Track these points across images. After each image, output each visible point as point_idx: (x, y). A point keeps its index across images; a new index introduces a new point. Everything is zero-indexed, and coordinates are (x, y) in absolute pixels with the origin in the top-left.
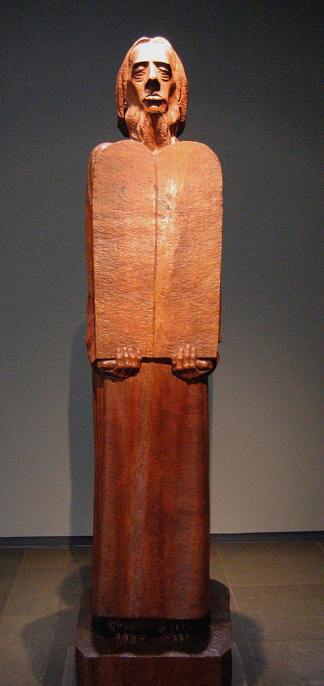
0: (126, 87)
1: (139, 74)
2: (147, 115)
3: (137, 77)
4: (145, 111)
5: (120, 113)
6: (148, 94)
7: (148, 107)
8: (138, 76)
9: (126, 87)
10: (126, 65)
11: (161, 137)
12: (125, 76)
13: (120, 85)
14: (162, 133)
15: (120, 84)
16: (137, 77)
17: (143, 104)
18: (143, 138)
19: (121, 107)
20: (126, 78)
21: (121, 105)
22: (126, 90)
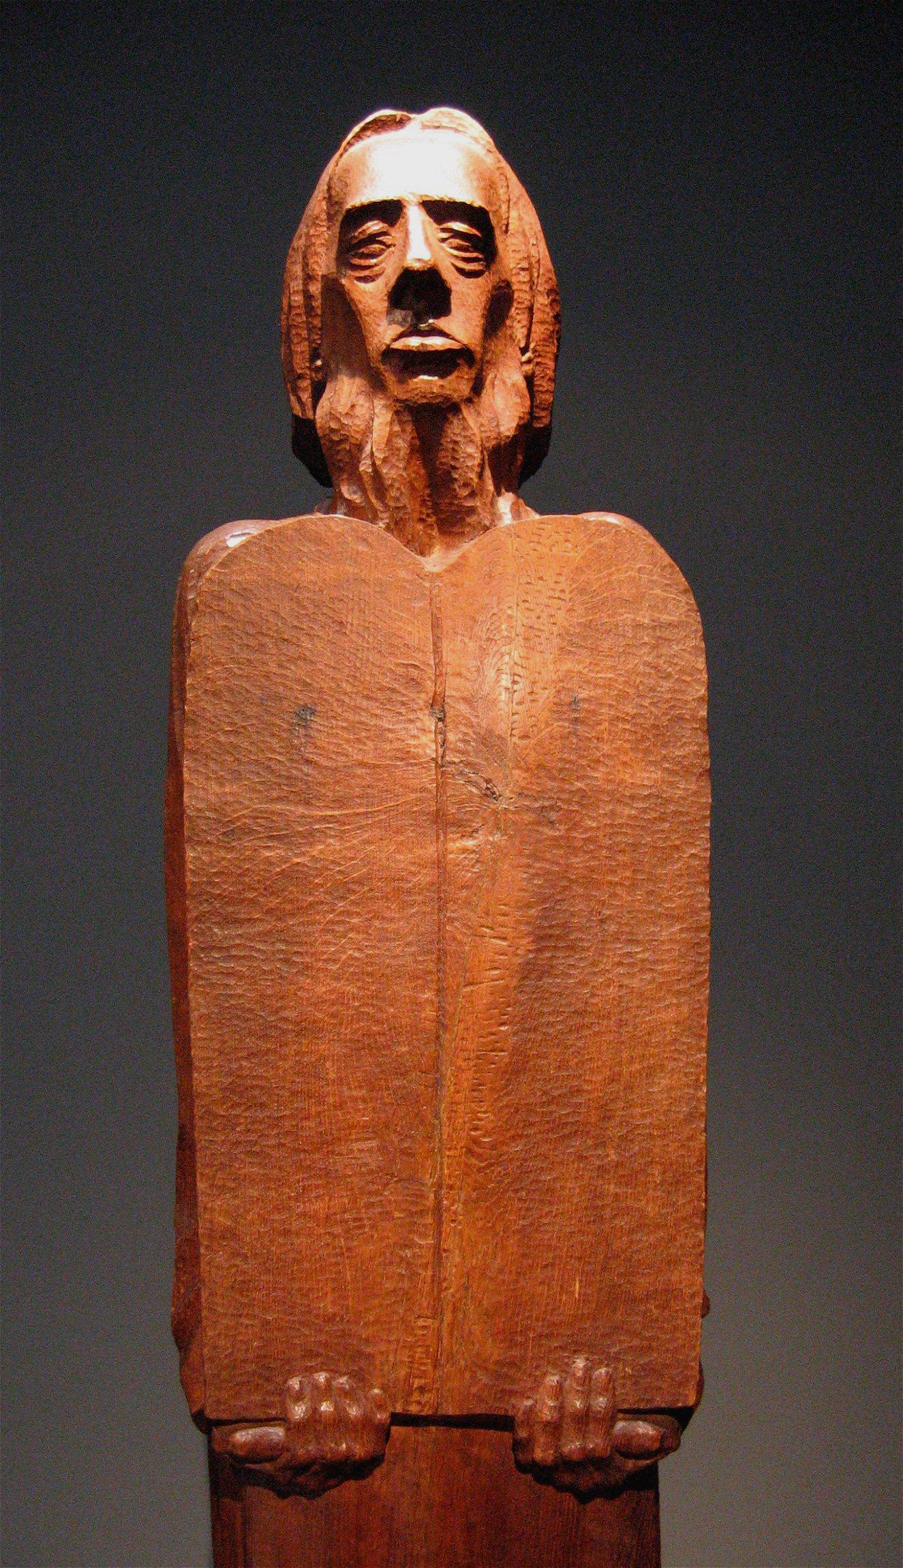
2: (397, 413)
3: (356, 261)
4: (388, 399)
5: (299, 399)
7: (401, 381)
9: (317, 303)
11: (456, 497)
12: (315, 259)
16: (356, 261)
17: (382, 367)
21: (299, 371)
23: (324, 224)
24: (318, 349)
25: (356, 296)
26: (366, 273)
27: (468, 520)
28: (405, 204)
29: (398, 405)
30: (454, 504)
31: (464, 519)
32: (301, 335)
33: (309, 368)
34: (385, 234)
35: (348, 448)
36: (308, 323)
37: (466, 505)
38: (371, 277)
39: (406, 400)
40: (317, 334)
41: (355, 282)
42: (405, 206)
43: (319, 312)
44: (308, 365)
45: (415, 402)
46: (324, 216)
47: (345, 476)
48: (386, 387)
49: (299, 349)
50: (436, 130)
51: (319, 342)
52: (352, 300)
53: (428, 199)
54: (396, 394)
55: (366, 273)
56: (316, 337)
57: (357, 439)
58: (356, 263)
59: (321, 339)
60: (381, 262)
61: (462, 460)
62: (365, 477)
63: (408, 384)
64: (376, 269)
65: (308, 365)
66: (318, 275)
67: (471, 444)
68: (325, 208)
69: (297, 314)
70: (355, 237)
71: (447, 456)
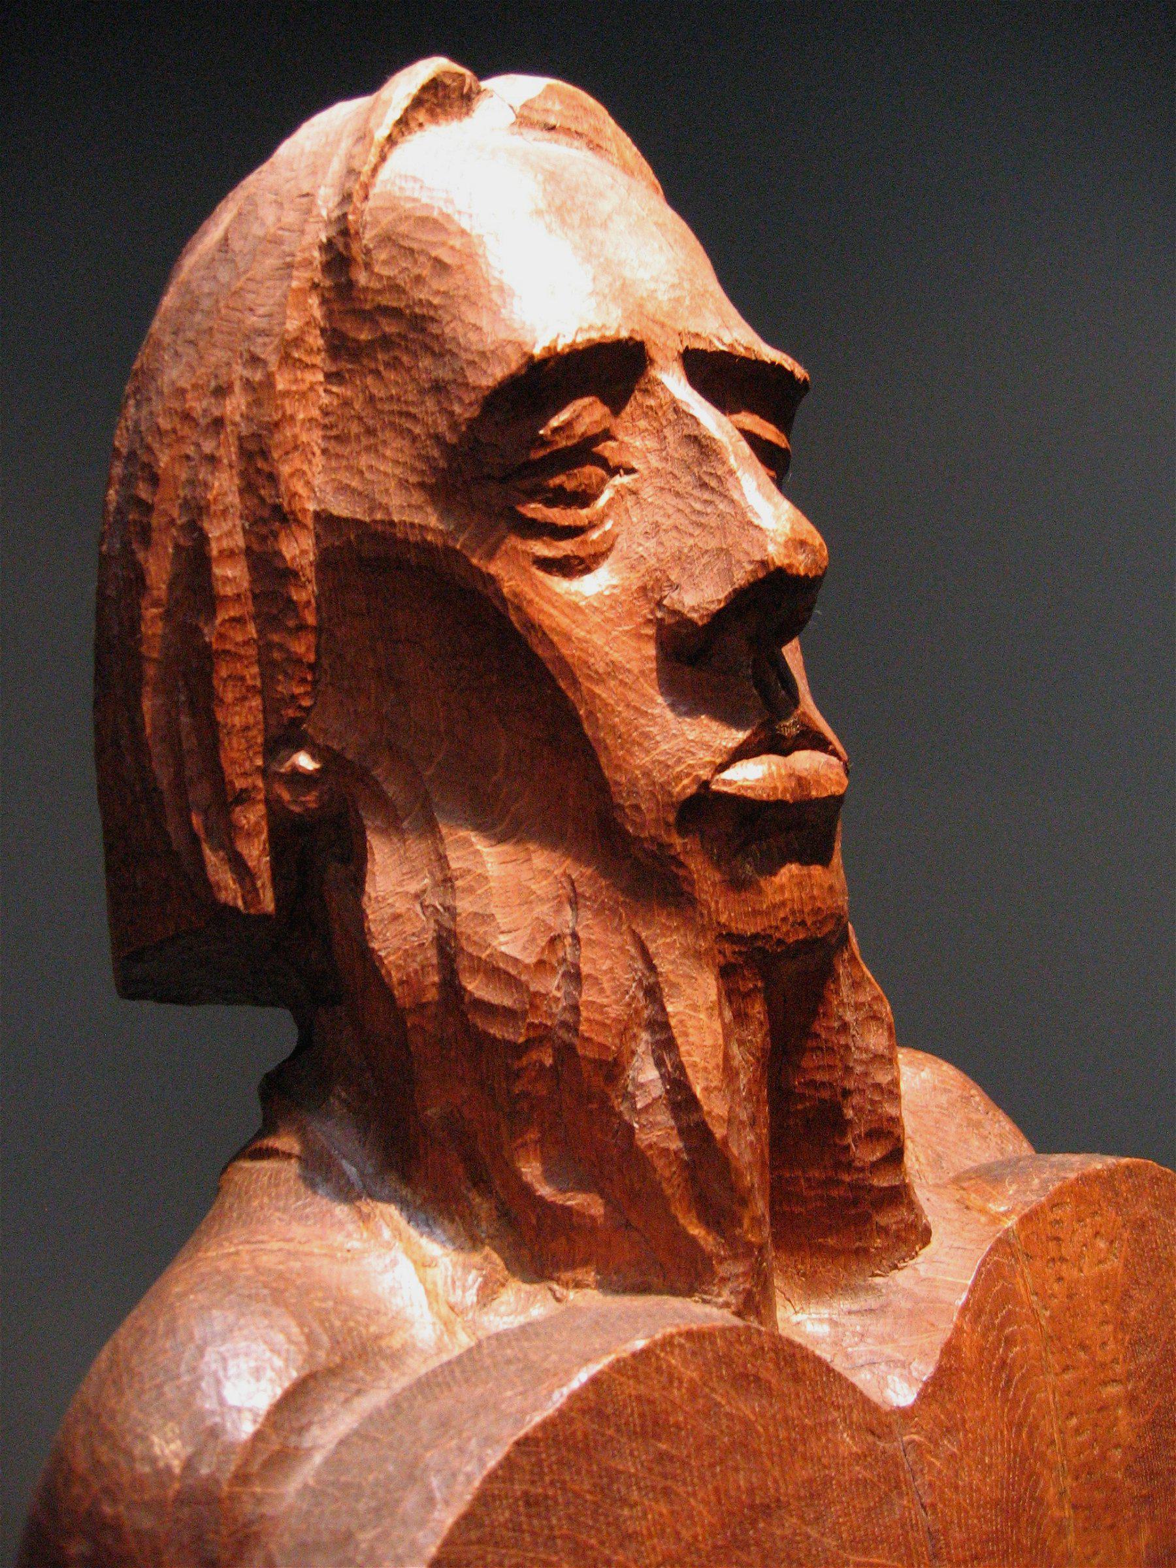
0: (312, 588)
1: (570, 485)
2: (726, 973)
3: (535, 510)
4: (702, 931)
5: (238, 863)
6: (741, 736)
7: (737, 885)
8: (550, 503)
9: (305, 594)
10: (298, 341)
11: (849, 1167)
12: (297, 461)
13: (230, 554)
14: (862, 1130)
15: (225, 544)
16: (535, 510)
17: (678, 841)
18: (732, 1242)
19: (243, 798)
20: (300, 487)
21: (240, 784)
22: (311, 619)
23: (317, 360)
24: (301, 721)
25: (552, 617)
26: (566, 547)
27: (883, 1219)
28: (653, 352)
29: (728, 948)
30: (840, 1182)
31: (868, 1218)
32: (242, 679)
33: (263, 772)
34: (607, 435)
35: (549, 1062)
36: (265, 648)
37: (875, 1182)
38: (582, 560)
39: (755, 936)
40: (303, 681)
41: (540, 574)
42: (652, 361)
43: (311, 619)
44: (259, 762)
45: (780, 942)
46: (316, 340)
47: (532, 1135)
48: (692, 902)
49: (237, 720)
50: (547, 135)
51: (306, 703)
52: (532, 626)
53: (700, 345)
54: (723, 919)
55: (566, 547)
56: (299, 690)
57: (604, 1047)
58: (538, 516)
59: (313, 693)
60: (603, 516)
61: (859, 1069)
62: (660, 1163)
63: (760, 892)
64: (595, 535)
65: (259, 762)
66: (304, 511)
67: (873, 1026)
68: (318, 313)
69: (233, 620)
70: (543, 442)
71: (832, 1068)
